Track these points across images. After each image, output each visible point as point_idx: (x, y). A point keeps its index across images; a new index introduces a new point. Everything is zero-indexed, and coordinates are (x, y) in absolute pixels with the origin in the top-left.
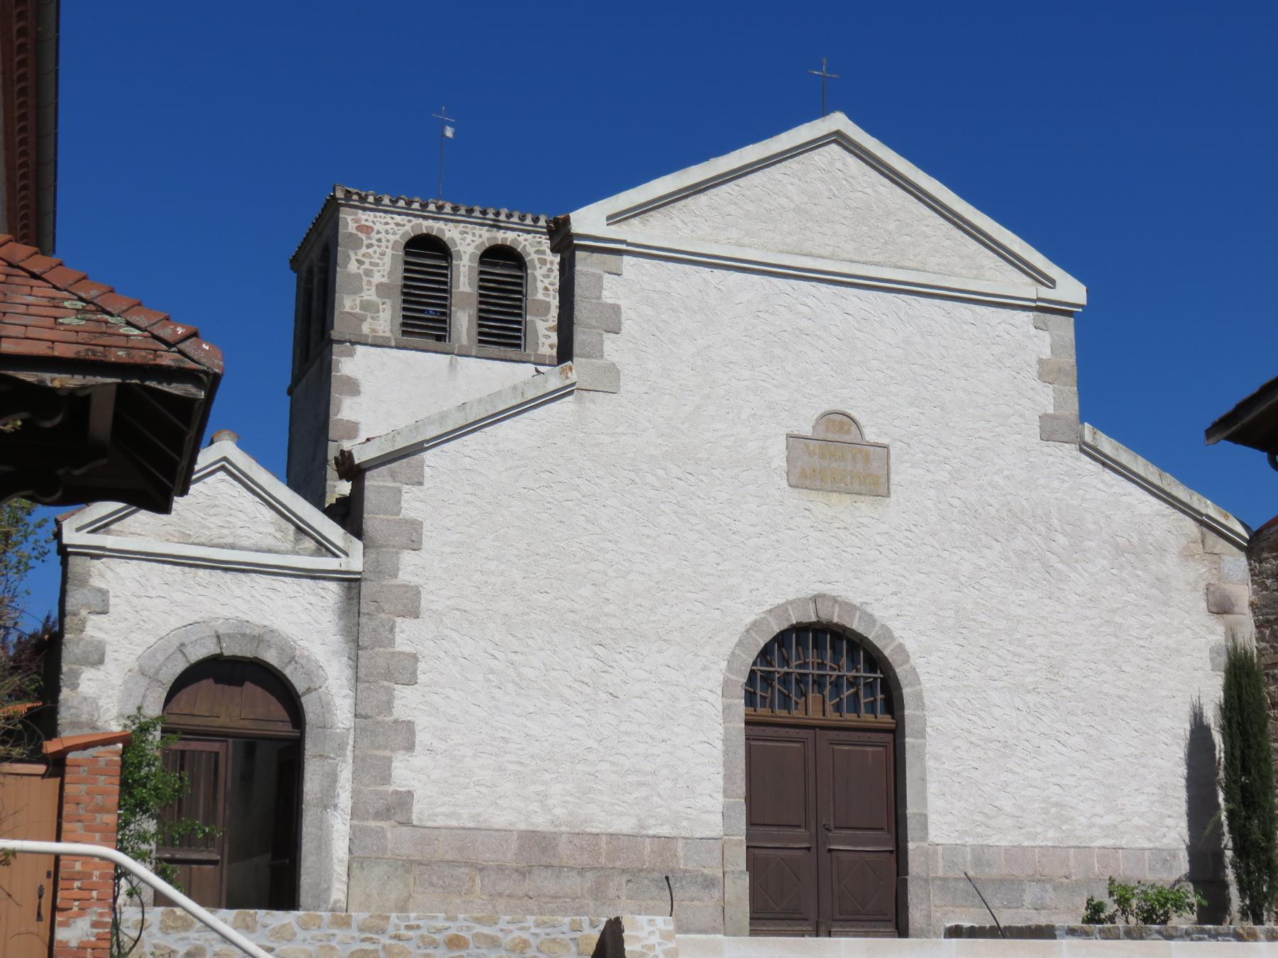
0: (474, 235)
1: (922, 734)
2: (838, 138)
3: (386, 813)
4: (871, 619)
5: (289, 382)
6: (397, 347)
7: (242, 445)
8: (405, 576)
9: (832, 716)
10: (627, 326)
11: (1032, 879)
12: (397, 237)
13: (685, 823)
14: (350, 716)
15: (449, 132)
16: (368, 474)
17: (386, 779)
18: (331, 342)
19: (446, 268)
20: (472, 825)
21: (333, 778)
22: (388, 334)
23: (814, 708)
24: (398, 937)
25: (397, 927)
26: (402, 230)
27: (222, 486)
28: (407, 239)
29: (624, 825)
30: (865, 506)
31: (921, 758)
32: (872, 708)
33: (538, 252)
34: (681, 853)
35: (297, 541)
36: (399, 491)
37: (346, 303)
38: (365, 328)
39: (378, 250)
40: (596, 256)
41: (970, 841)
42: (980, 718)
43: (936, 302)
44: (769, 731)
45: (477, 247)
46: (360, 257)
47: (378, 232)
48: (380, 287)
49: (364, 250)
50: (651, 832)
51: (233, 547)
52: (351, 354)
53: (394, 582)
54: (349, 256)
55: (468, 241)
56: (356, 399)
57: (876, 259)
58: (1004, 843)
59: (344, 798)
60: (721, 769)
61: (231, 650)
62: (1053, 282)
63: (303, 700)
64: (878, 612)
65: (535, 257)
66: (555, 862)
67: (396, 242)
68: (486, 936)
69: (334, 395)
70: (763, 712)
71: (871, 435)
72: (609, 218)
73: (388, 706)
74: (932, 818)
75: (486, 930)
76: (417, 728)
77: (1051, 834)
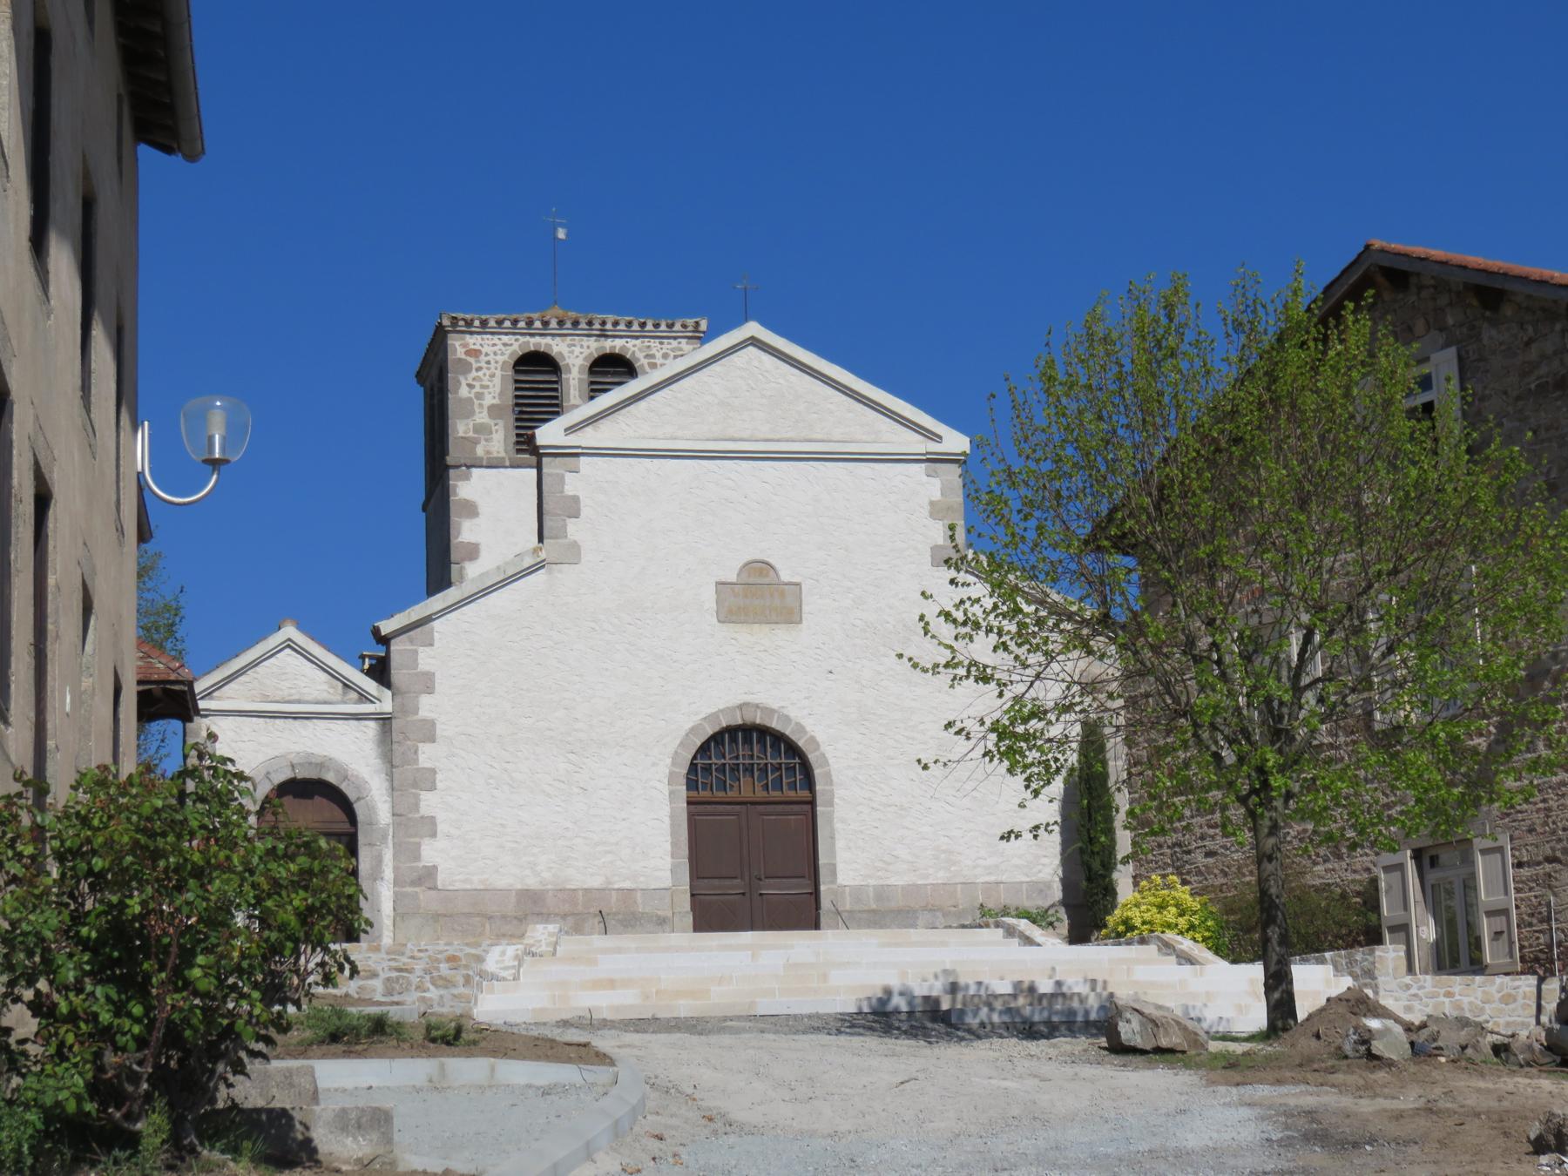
0: (582, 346)
1: (831, 803)
2: (754, 342)
3: (418, 882)
4: (787, 719)
5: (423, 498)
6: (512, 466)
7: (300, 628)
8: (424, 713)
9: (761, 794)
10: (585, 512)
11: (925, 908)
12: (506, 358)
13: (642, 879)
14: (389, 815)
15: (561, 234)
16: (393, 642)
17: (417, 858)
18: (447, 467)
19: (556, 382)
20: (482, 887)
21: (379, 860)
22: (503, 454)
23: (747, 788)
24: (413, 957)
25: (412, 951)
26: (509, 350)
27: (289, 659)
28: (515, 358)
29: (596, 882)
30: (781, 634)
31: (830, 821)
32: (793, 786)
33: (647, 356)
34: (639, 900)
35: (344, 694)
36: (416, 652)
37: (460, 428)
38: (480, 451)
39: (488, 373)
40: (559, 459)
41: (872, 882)
42: (881, 789)
43: (840, 464)
44: (709, 808)
45: (585, 359)
46: (470, 382)
47: (487, 355)
48: (491, 408)
49: (474, 374)
50: (616, 886)
51: (299, 702)
52: (467, 478)
53: (415, 718)
54: (459, 382)
55: (576, 353)
56: (476, 521)
57: (789, 435)
58: (901, 883)
59: (388, 873)
60: (669, 838)
61: (301, 774)
62: (940, 437)
63: (355, 806)
64: (793, 713)
65: (645, 362)
66: (545, 911)
67: (504, 362)
68: (473, 955)
69: (454, 519)
70: (704, 794)
71: (785, 576)
72: (566, 430)
73: (416, 806)
74: (840, 867)
75: (473, 951)
76: (438, 821)
77: (941, 874)
